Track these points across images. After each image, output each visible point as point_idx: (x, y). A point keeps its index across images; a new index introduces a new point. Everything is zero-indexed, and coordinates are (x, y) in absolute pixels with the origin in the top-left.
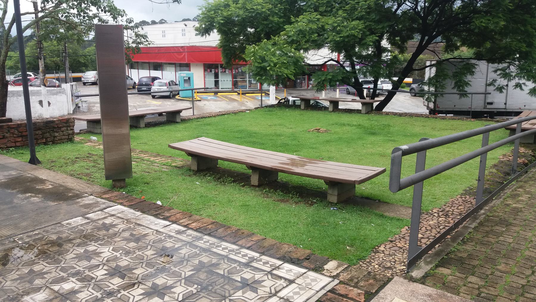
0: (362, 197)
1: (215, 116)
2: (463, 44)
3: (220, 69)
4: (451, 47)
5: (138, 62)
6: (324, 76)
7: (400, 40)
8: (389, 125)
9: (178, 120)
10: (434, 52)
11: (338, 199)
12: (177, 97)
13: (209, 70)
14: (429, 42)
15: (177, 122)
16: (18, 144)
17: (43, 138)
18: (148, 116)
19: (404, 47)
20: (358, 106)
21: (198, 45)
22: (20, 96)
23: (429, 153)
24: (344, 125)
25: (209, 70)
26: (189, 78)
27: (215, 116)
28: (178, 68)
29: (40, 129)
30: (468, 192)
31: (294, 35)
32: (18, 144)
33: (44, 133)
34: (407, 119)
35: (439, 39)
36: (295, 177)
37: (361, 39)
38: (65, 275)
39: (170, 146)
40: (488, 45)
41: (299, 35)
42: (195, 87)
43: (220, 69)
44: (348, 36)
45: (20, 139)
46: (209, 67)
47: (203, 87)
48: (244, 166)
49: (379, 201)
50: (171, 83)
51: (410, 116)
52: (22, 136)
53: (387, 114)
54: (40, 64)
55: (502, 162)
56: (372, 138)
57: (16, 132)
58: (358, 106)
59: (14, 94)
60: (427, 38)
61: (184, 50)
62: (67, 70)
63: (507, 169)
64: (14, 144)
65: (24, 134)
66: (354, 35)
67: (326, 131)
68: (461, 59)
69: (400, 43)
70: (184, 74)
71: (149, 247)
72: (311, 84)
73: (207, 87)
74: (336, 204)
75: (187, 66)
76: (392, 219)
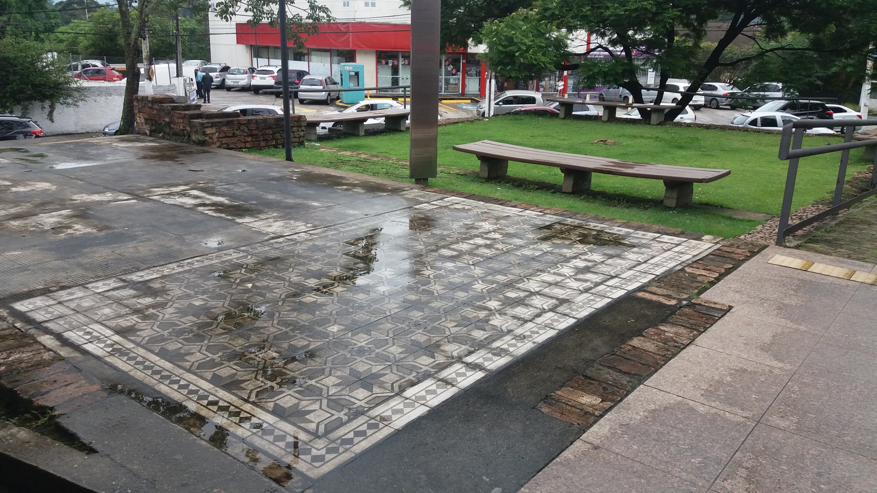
0: (701, 204)
1: (445, 125)
2: (793, 28)
3: (401, 59)
4: (774, 31)
5: (268, 47)
6: (589, 72)
7: (696, 20)
8: (697, 139)
9: (403, 128)
10: (754, 39)
11: (677, 203)
12: (338, 102)
13: (384, 62)
14: (745, 23)
15: (401, 131)
16: (248, 145)
17: (273, 139)
18: (322, 125)
19: (701, 31)
20: (636, 115)
21: (367, 21)
22: (120, 95)
23: (802, 161)
24: (635, 137)
25: (384, 62)
26: (357, 74)
27: (445, 125)
28: (335, 59)
29: (270, 128)
30: (822, 202)
31: (556, 7)
32: (248, 145)
33: (274, 133)
34: (719, 133)
35: (757, 20)
36: (639, 182)
37: (656, 14)
38: (192, 293)
39: (455, 148)
40: (832, 28)
41: (562, 7)
42: (366, 87)
43: (401, 59)
44: (636, 10)
45: (249, 139)
46: (383, 57)
47: (375, 86)
48: (558, 171)
49: (722, 207)
50: (330, 81)
51: (559, 147)
52: (251, 135)
53: (679, 124)
54: (144, 47)
55: (857, 178)
56: (683, 153)
57: (246, 130)
58: (636, 115)
59: (101, 92)
60: (742, 16)
61: (348, 27)
62: (180, 57)
63: (863, 185)
64: (243, 145)
65: (255, 132)
66: (646, 9)
67: (614, 144)
68: (794, 49)
69: (696, 24)
70: (349, 67)
71: (238, 281)
72: (543, 87)
73: (380, 86)
74: (675, 208)
75: (350, 57)
76: (741, 220)
